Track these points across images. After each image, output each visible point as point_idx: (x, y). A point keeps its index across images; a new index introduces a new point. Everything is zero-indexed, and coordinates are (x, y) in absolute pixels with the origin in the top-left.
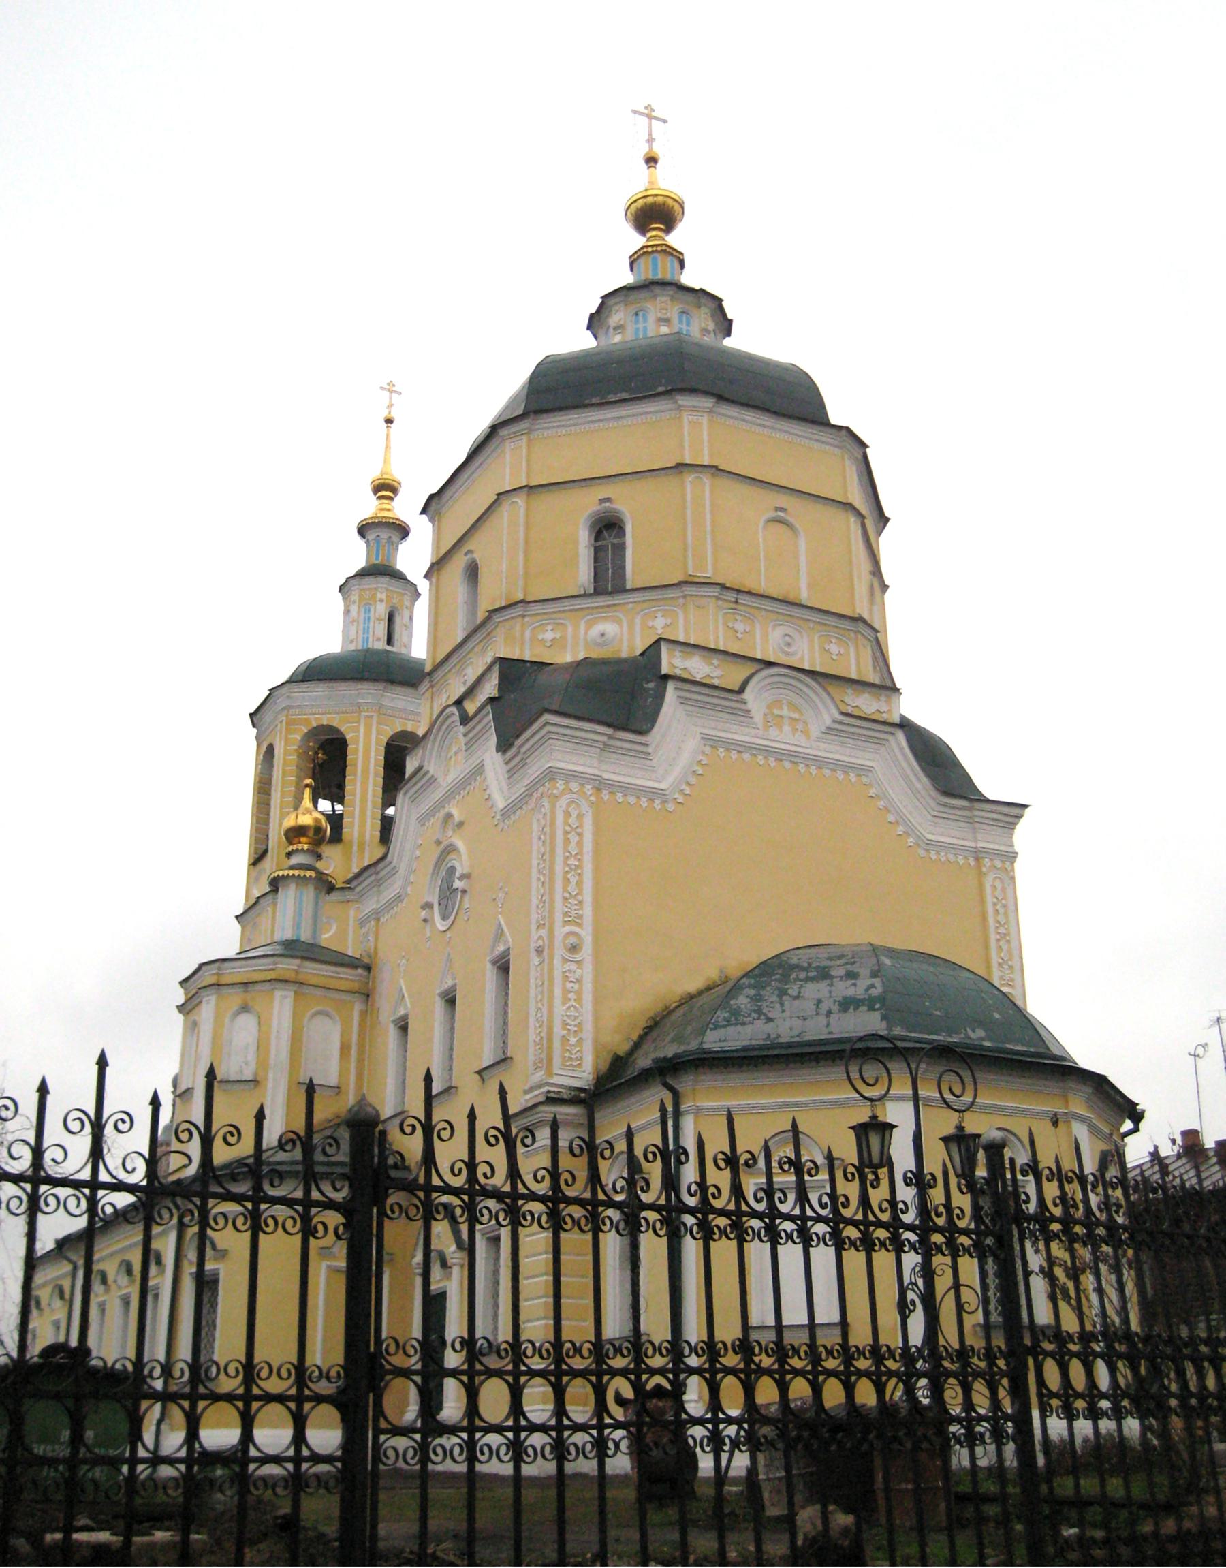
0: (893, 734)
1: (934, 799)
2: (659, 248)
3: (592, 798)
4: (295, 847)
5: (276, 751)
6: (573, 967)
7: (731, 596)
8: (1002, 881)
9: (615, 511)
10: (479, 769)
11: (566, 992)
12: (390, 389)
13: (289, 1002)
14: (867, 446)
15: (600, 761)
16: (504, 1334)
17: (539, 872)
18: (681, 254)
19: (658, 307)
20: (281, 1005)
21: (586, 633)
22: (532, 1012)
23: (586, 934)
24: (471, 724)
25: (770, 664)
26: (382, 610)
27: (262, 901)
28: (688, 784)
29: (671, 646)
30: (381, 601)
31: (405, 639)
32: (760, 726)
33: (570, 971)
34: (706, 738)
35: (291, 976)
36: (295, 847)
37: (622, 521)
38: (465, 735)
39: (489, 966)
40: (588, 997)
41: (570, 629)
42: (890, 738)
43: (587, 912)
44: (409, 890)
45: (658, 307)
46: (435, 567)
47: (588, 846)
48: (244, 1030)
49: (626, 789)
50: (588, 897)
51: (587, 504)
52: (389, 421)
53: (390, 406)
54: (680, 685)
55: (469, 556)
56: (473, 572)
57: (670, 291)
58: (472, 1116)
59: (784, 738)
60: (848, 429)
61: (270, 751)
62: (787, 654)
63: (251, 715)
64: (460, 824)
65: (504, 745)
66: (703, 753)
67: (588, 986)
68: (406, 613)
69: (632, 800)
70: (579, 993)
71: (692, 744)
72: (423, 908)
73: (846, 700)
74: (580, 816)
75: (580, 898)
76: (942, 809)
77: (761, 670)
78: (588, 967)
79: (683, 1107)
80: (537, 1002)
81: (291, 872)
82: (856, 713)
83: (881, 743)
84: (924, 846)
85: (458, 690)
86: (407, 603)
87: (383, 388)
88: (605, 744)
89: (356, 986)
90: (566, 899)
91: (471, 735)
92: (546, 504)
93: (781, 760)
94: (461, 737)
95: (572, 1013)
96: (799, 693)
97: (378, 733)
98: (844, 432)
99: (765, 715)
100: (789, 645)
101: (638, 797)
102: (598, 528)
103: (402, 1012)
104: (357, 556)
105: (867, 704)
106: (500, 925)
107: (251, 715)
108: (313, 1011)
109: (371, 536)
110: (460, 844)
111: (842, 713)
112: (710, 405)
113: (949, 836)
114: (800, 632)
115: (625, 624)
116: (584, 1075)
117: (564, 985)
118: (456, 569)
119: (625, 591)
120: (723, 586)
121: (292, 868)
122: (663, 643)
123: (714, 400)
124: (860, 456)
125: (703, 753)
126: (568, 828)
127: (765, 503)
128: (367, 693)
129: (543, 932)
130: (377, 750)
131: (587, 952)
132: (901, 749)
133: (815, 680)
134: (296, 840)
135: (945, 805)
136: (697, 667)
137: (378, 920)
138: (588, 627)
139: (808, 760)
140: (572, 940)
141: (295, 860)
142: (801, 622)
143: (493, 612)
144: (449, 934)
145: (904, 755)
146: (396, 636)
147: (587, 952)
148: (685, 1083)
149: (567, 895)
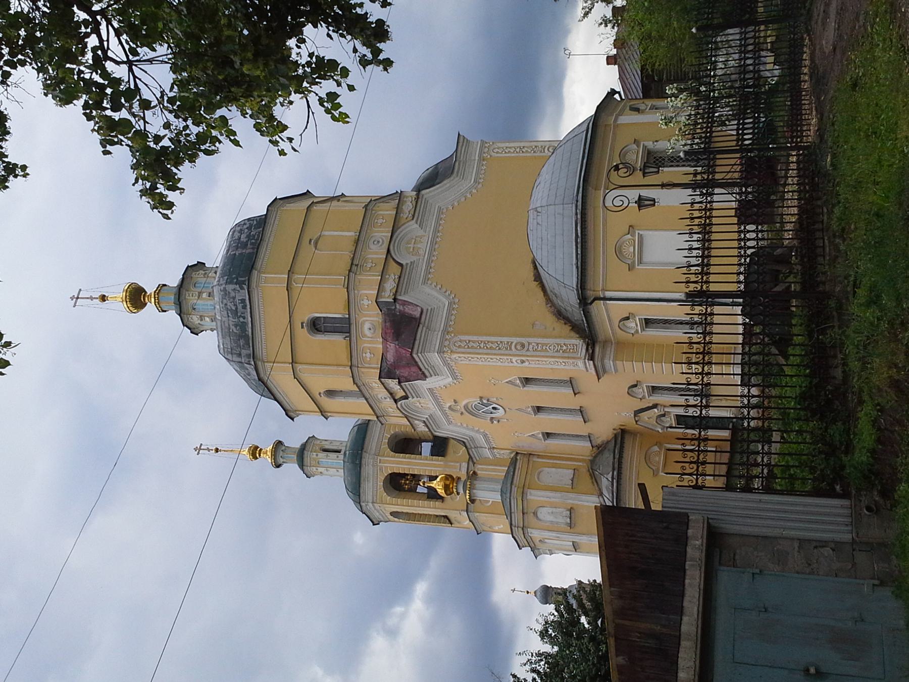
0: (423, 195)
1: (454, 178)
2: (157, 296)
3: (452, 335)
4: (455, 490)
5: (395, 510)
6: (531, 346)
7: (354, 268)
8: (494, 149)
9: (308, 320)
10: (431, 390)
11: (542, 350)
12: (198, 450)
13: (533, 492)
14: (276, 198)
15: (435, 331)
16: (712, 238)
17: (485, 361)
18: (159, 285)
19: (191, 298)
20: (535, 496)
21: (369, 337)
22: (550, 366)
23: (515, 340)
24: (409, 395)
25: (388, 251)
26: (322, 455)
27: (471, 519)
28: (445, 292)
29: (379, 297)
30: (317, 455)
31: (338, 444)
32: (418, 258)
33: (533, 348)
34: (424, 283)
35: (520, 490)
36: (455, 490)
37: (313, 318)
38: (413, 398)
39: (525, 388)
40: (545, 341)
41: (365, 345)
42: (425, 197)
43: (505, 339)
44: (482, 431)
45: (191, 298)
46: (323, 414)
47: (475, 338)
48: (544, 513)
49: (448, 319)
50: (499, 339)
51: (303, 334)
52: (217, 450)
53: (208, 450)
54: (398, 294)
55: (322, 395)
56: (330, 393)
57: (183, 291)
58: (688, 225)
59: (424, 246)
60: (268, 206)
61: (394, 514)
62: (383, 243)
63: (374, 525)
64: (455, 402)
65: (424, 377)
66: (431, 284)
67: (539, 340)
68: (324, 443)
69: (453, 317)
70: (543, 345)
71: (427, 289)
72: (492, 422)
73: (405, 217)
74: (461, 341)
75: (499, 343)
76: (459, 174)
77: (392, 257)
78: (531, 340)
79: (602, 296)
80: (547, 364)
81: (468, 494)
82: (412, 212)
83: (426, 202)
84: (477, 184)
85: (389, 401)
86: (318, 442)
87: (198, 453)
88: (427, 328)
89: (526, 459)
90: (499, 349)
91: (414, 395)
92: (301, 355)
93: (435, 249)
94: (414, 400)
95: (552, 348)
96: (402, 239)
97: (389, 457)
98: (270, 208)
99: (413, 255)
100: (378, 242)
101: (452, 315)
102: (316, 331)
103: (541, 435)
104: (291, 468)
105: (408, 206)
106: (507, 382)
107: (374, 525)
108: (536, 479)
109: (281, 460)
110: (464, 403)
111: (413, 219)
112: (256, 272)
113: (472, 172)
114: (372, 237)
115: (365, 319)
116: (581, 343)
117: (539, 351)
118: (326, 402)
119: (349, 318)
120: (350, 271)
121: (465, 493)
122: (378, 300)
123: (254, 271)
124: (282, 202)
125: (431, 284)
126: (466, 347)
127: (307, 250)
128: (368, 462)
129: (514, 359)
130: (397, 457)
131: (524, 340)
132: (430, 192)
133: (396, 231)
134: (451, 490)
135: (458, 172)
136: (390, 285)
137: (494, 448)
138: (364, 336)
139: (435, 236)
140: (519, 347)
141: (461, 491)
142: (367, 236)
143: (354, 383)
144: (507, 409)
145: (434, 190)
146: (335, 448)
147: (524, 340)
148: (590, 294)
149: (497, 348)
